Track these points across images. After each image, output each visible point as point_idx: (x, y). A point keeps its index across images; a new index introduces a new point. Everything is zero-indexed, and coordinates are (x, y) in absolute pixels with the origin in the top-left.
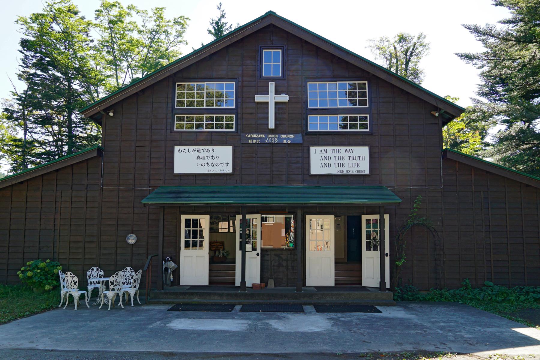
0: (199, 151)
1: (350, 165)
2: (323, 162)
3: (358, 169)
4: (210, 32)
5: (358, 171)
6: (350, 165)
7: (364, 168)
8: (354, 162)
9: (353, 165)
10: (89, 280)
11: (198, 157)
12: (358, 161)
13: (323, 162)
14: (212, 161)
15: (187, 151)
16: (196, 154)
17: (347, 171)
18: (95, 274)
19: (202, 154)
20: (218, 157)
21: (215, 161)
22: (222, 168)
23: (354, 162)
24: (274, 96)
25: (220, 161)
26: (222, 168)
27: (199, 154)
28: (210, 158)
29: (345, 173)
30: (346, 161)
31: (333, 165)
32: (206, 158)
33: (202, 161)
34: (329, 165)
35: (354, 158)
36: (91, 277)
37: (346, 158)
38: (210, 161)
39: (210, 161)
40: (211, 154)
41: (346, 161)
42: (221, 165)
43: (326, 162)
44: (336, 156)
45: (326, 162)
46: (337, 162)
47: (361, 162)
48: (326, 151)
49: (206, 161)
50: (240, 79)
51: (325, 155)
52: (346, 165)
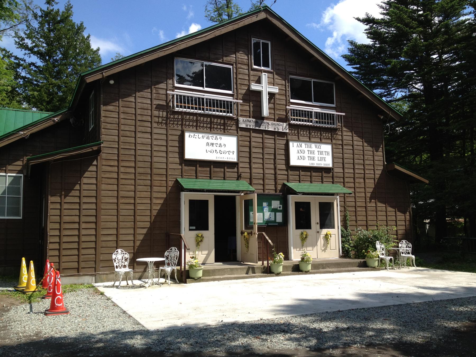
0: (208, 138)
1: (319, 159)
2: (299, 155)
3: (325, 162)
4: (17, 48)
5: (312, 164)
6: (319, 159)
7: (328, 162)
8: (322, 156)
9: (322, 159)
10: (115, 265)
11: (208, 144)
12: (324, 156)
13: (299, 155)
14: (220, 148)
15: (197, 137)
16: (206, 141)
17: (317, 164)
18: (120, 257)
19: (210, 141)
20: (225, 145)
21: (223, 149)
22: (229, 156)
23: (322, 156)
24: (263, 89)
25: (227, 149)
26: (229, 156)
27: (208, 141)
28: (218, 146)
29: (315, 165)
30: (316, 155)
31: (307, 158)
32: (214, 145)
33: (210, 148)
34: (303, 158)
35: (321, 153)
36: (117, 260)
37: (316, 153)
38: (218, 149)
39: (218, 149)
40: (219, 141)
41: (316, 155)
42: (227, 153)
43: (302, 155)
44: (308, 151)
45: (302, 155)
46: (310, 155)
47: (327, 156)
48: (301, 146)
49: (214, 148)
50: (234, 65)
51: (301, 148)
52: (316, 159)
